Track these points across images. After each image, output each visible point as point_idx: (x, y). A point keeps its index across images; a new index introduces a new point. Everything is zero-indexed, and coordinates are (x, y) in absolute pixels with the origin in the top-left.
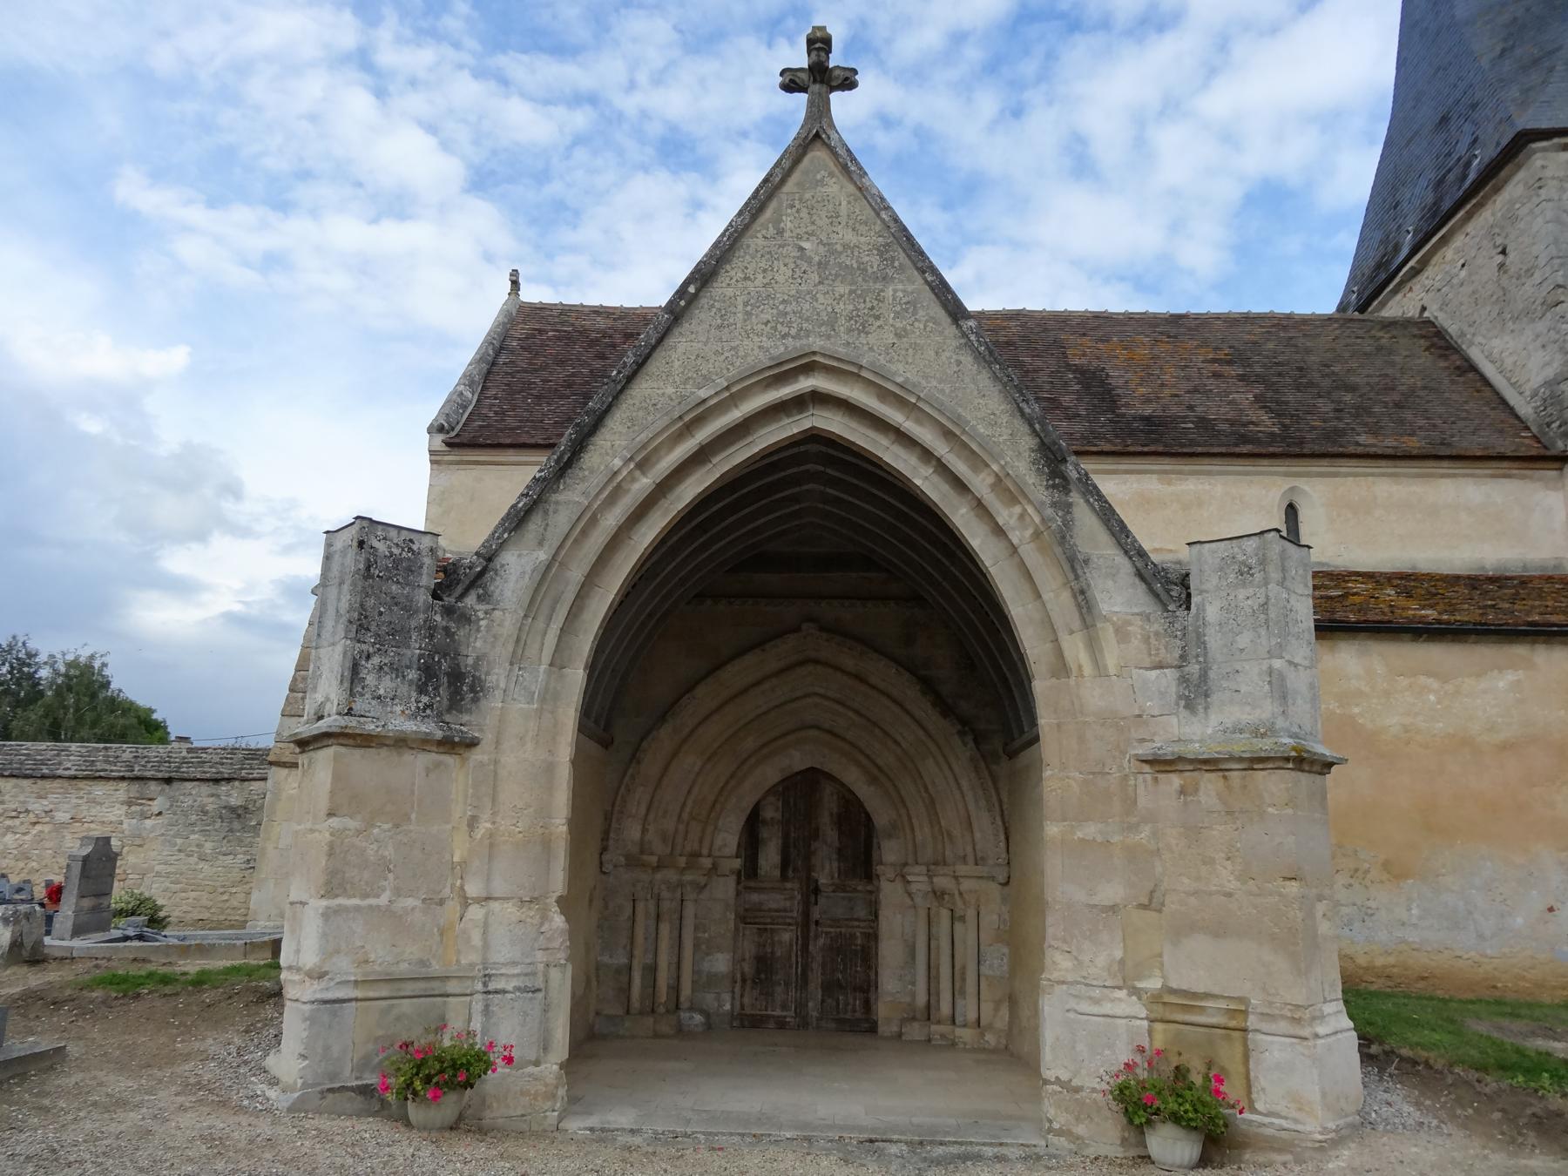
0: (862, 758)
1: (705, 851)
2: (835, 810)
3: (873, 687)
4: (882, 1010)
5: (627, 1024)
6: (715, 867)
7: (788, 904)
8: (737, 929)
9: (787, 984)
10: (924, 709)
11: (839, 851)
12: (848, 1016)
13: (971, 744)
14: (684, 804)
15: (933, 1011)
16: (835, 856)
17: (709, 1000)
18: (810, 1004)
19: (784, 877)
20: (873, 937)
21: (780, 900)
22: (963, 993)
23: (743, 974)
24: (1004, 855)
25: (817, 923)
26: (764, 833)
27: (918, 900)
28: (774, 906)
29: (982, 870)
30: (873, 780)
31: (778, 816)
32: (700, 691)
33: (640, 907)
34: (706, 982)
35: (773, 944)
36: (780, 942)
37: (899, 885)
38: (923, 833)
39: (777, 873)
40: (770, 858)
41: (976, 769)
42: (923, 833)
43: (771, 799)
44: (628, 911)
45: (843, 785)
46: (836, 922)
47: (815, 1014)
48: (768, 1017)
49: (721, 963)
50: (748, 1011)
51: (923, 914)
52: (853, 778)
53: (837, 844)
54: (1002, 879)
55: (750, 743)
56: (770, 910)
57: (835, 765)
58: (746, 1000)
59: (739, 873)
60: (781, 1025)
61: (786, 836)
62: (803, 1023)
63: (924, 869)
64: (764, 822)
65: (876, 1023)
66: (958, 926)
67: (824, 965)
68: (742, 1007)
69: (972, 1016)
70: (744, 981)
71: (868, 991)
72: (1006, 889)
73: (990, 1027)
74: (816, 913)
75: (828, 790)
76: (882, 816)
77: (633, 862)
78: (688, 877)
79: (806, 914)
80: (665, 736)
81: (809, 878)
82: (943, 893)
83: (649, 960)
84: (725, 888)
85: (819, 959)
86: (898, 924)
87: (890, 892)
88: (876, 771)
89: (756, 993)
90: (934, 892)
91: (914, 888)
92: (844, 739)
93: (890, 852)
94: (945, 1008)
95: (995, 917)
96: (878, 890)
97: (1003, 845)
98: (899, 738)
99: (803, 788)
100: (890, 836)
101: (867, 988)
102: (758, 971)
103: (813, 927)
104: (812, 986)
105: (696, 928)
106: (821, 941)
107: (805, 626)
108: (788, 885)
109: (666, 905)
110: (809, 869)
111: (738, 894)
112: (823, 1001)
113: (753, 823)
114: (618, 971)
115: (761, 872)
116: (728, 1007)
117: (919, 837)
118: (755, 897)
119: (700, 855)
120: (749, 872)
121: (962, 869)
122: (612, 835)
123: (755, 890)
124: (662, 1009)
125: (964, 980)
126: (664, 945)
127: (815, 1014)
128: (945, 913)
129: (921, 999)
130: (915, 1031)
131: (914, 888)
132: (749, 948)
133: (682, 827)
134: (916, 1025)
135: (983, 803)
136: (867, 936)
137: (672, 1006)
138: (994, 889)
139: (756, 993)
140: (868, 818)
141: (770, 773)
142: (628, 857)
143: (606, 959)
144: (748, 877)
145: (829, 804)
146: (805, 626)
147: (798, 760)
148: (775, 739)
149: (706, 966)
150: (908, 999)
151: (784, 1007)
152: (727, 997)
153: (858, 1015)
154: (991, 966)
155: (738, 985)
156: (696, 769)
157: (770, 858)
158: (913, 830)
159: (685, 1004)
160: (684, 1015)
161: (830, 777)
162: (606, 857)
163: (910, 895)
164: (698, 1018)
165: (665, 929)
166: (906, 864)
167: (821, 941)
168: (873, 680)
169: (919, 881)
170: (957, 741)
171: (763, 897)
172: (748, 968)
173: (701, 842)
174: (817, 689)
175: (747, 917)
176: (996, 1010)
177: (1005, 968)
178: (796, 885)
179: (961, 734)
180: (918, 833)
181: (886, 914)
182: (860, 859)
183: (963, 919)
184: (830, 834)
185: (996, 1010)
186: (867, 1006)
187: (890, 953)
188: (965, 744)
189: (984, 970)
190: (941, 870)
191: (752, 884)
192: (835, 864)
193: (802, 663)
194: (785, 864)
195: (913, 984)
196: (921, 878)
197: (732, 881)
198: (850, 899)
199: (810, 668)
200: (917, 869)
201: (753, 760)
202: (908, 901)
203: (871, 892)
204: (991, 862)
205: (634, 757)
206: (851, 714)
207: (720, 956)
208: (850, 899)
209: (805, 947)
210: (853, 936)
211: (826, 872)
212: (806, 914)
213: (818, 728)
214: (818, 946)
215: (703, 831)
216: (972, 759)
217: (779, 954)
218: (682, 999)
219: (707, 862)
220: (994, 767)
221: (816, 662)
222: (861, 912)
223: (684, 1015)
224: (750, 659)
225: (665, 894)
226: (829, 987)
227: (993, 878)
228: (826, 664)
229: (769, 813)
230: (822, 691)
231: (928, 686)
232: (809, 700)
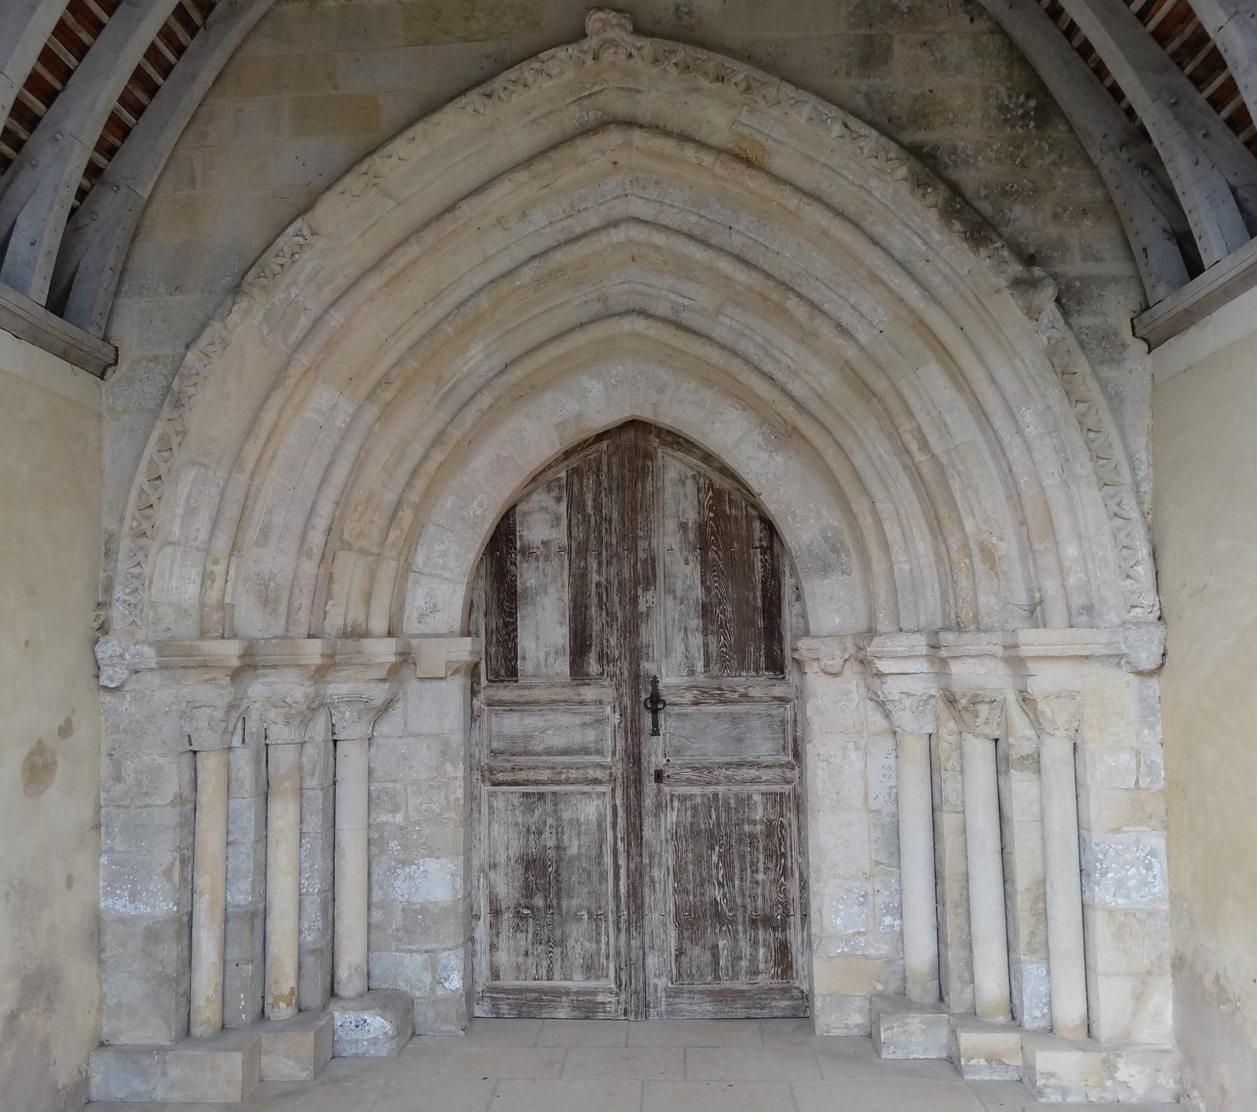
0: (762, 388)
1: (379, 624)
2: (692, 516)
3: (779, 180)
4: (824, 974)
5: (174, 1072)
6: (406, 658)
7: (591, 735)
8: (472, 797)
9: (596, 918)
10: (920, 228)
11: (706, 611)
12: (740, 985)
13: (1050, 311)
14: (312, 510)
15: (954, 985)
16: (695, 623)
17: (409, 969)
18: (652, 961)
19: (578, 672)
20: (792, 802)
21: (571, 725)
22: (1044, 950)
23: (493, 899)
24: (1149, 598)
25: (659, 776)
26: (528, 576)
27: (905, 718)
28: (556, 741)
29: (1097, 641)
30: (784, 435)
31: (559, 536)
32: (329, 211)
33: (210, 766)
34: (419, 921)
35: (558, 830)
36: (575, 823)
37: (852, 681)
38: (913, 552)
39: (562, 666)
40: (544, 631)
41: (1066, 374)
42: (913, 552)
43: (541, 498)
44: (173, 781)
45: (707, 457)
46: (703, 771)
47: (663, 982)
48: (557, 993)
49: (435, 882)
50: (508, 982)
51: (916, 750)
52: (733, 437)
53: (698, 592)
54: (1147, 660)
55: (476, 358)
56: (548, 752)
57: (681, 407)
58: (503, 957)
59: (474, 671)
60: (587, 1009)
61: (579, 583)
62: (639, 1005)
63: (920, 643)
64: (527, 552)
65: (806, 998)
66: (1021, 786)
67: (679, 872)
68: (495, 975)
69: (1070, 1011)
70: (496, 913)
71: (784, 925)
72: (1154, 684)
73: (1123, 1045)
74: (655, 754)
75: (673, 470)
76: (803, 518)
77: (176, 658)
78: (338, 688)
79: (634, 758)
80: (246, 325)
81: (636, 676)
82: (975, 701)
83: (242, 896)
84: (438, 707)
85: (669, 859)
86: (856, 771)
87: (831, 701)
88: (790, 411)
89: (524, 941)
90: (951, 701)
91: (893, 688)
92: (708, 338)
93: (825, 608)
94: (991, 984)
95: (1126, 758)
96: (801, 694)
97: (1144, 571)
98: (846, 317)
99: (618, 461)
100: (825, 569)
101: (781, 923)
102: (528, 891)
103: (650, 786)
104: (653, 918)
105: (371, 802)
106: (671, 818)
107: (594, 21)
108: (589, 693)
109: (283, 759)
110: (636, 654)
111: (473, 717)
112: (680, 953)
113: (502, 546)
114: (153, 935)
115: (526, 667)
116: (455, 983)
117: (903, 567)
118: (512, 724)
119: (366, 634)
120: (501, 660)
121: (1032, 640)
122: (119, 593)
123: (511, 706)
124: (283, 1011)
125: (1043, 916)
126: (283, 856)
127: (663, 982)
128: (980, 753)
129: (921, 953)
130: (914, 1038)
131: (893, 688)
132: (502, 837)
133: (309, 567)
134: (915, 1022)
135: (1083, 466)
136: (777, 800)
137: (313, 996)
138: (1121, 689)
139: (524, 941)
140: (770, 527)
141: (536, 435)
142: (162, 647)
143: (118, 905)
144: (495, 679)
145: (676, 499)
146: (594, 21)
147: (597, 402)
148: (541, 346)
149: (401, 889)
150: (885, 949)
151: (590, 969)
152: (453, 962)
153: (763, 981)
154: (1120, 884)
155: (482, 931)
156: (340, 422)
157: (544, 631)
158: (886, 547)
159: (349, 983)
160: (342, 1017)
161: (677, 441)
162: (107, 649)
163: (881, 705)
164: (378, 1024)
165: (284, 814)
166: (871, 633)
167: (671, 818)
168: (781, 163)
169: (907, 675)
170: (1009, 308)
171: (531, 722)
172: (506, 887)
173: (368, 598)
174: (638, 208)
175: (495, 770)
176: (1139, 997)
177: (1160, 887)
178: (608, 694)
179: (1021, 285)
180: (899, 555)
181: (819, 749)
182: (756, 625)
183: (1034, 763)
184: (682, 571)
185: (1139, 997)
186: (783, 958)
187: (837, 842)
188: (1032, 313)
189: (1103, 894)
190: (973, 642)
191: (504, 693)
192: (696, 640)
193: (588, 131)
194: (580, 645)
195: (899, 912)
196: (911, 666)
197: (455, 689)
198: (735, 720)
199: (614, 137)
200: (903, 644)
201: (485, 401)
202: (877, 718)
203: (783, 700)
204: (1112, 617)
205: (172, 399)
206: (725, 265)
207: (431, 865)
208: (735, 720)
209: (634, 832)
210: (744, 802)
211: (675, 648)
212: (634, 758)
213: (644, 313)
214: (661, 829)
215: (372, 577)
216: (1051, 354)
217: (573, 850)
218: (343, 973)
219: (383, 651)
220: (1107, 372)
221: (629, 123)
222: (763, 746)
223: (342, 1017)
224: (452, 124)
225: (280, 732)
226: (689, 922)
227: (1117, 659)
228: (658, 129)
229: (542, 527)
230: (647, 212)
231: (929, 166)
232: (618, 235)
